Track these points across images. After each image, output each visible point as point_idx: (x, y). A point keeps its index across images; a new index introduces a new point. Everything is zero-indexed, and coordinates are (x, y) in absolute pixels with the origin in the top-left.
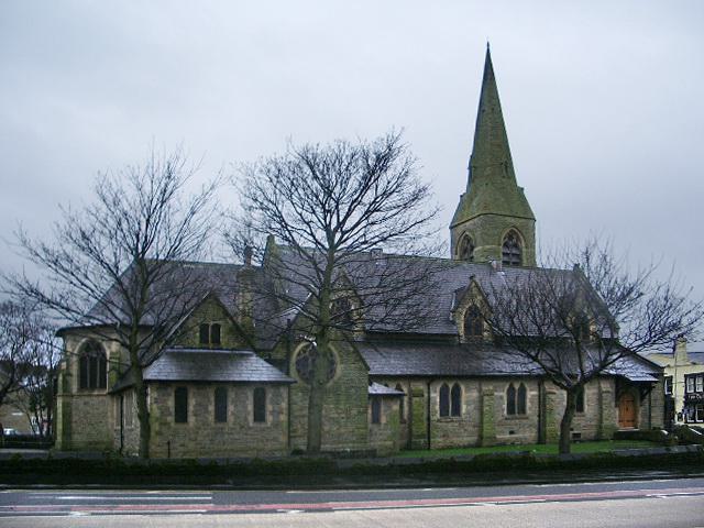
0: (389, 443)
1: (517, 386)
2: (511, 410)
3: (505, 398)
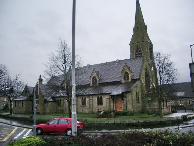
0: (49, 111)
1: (100, 96)
2: (83, 104)
3: (81, 101)
